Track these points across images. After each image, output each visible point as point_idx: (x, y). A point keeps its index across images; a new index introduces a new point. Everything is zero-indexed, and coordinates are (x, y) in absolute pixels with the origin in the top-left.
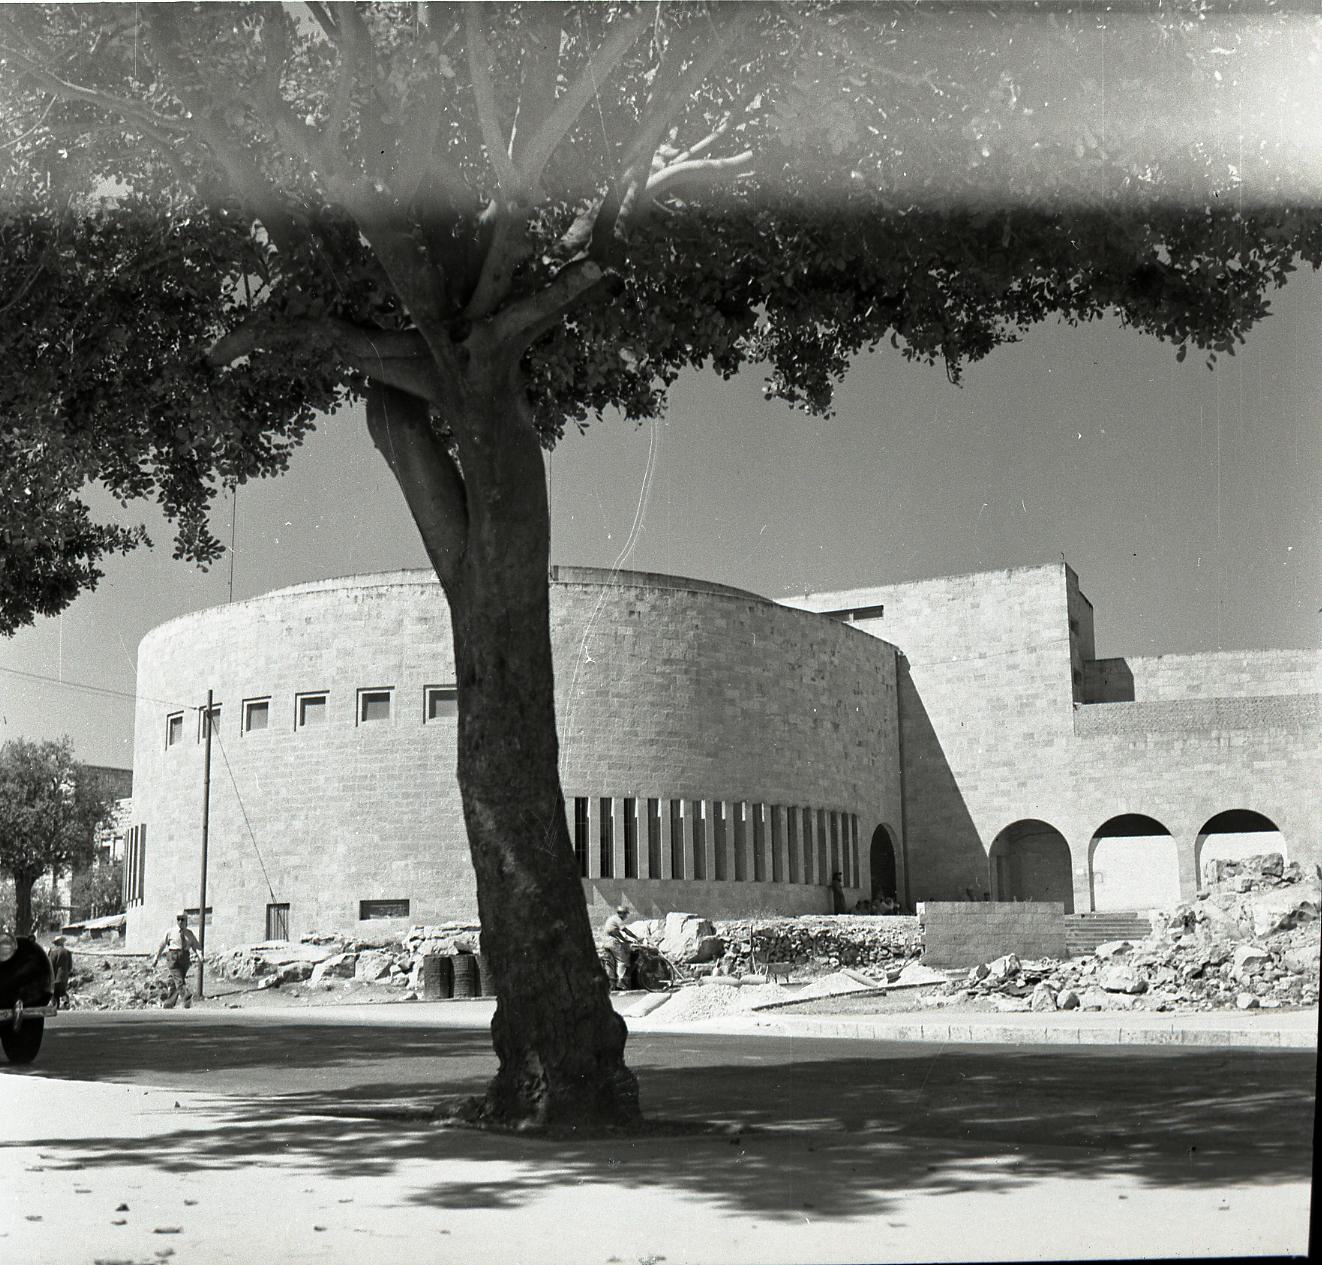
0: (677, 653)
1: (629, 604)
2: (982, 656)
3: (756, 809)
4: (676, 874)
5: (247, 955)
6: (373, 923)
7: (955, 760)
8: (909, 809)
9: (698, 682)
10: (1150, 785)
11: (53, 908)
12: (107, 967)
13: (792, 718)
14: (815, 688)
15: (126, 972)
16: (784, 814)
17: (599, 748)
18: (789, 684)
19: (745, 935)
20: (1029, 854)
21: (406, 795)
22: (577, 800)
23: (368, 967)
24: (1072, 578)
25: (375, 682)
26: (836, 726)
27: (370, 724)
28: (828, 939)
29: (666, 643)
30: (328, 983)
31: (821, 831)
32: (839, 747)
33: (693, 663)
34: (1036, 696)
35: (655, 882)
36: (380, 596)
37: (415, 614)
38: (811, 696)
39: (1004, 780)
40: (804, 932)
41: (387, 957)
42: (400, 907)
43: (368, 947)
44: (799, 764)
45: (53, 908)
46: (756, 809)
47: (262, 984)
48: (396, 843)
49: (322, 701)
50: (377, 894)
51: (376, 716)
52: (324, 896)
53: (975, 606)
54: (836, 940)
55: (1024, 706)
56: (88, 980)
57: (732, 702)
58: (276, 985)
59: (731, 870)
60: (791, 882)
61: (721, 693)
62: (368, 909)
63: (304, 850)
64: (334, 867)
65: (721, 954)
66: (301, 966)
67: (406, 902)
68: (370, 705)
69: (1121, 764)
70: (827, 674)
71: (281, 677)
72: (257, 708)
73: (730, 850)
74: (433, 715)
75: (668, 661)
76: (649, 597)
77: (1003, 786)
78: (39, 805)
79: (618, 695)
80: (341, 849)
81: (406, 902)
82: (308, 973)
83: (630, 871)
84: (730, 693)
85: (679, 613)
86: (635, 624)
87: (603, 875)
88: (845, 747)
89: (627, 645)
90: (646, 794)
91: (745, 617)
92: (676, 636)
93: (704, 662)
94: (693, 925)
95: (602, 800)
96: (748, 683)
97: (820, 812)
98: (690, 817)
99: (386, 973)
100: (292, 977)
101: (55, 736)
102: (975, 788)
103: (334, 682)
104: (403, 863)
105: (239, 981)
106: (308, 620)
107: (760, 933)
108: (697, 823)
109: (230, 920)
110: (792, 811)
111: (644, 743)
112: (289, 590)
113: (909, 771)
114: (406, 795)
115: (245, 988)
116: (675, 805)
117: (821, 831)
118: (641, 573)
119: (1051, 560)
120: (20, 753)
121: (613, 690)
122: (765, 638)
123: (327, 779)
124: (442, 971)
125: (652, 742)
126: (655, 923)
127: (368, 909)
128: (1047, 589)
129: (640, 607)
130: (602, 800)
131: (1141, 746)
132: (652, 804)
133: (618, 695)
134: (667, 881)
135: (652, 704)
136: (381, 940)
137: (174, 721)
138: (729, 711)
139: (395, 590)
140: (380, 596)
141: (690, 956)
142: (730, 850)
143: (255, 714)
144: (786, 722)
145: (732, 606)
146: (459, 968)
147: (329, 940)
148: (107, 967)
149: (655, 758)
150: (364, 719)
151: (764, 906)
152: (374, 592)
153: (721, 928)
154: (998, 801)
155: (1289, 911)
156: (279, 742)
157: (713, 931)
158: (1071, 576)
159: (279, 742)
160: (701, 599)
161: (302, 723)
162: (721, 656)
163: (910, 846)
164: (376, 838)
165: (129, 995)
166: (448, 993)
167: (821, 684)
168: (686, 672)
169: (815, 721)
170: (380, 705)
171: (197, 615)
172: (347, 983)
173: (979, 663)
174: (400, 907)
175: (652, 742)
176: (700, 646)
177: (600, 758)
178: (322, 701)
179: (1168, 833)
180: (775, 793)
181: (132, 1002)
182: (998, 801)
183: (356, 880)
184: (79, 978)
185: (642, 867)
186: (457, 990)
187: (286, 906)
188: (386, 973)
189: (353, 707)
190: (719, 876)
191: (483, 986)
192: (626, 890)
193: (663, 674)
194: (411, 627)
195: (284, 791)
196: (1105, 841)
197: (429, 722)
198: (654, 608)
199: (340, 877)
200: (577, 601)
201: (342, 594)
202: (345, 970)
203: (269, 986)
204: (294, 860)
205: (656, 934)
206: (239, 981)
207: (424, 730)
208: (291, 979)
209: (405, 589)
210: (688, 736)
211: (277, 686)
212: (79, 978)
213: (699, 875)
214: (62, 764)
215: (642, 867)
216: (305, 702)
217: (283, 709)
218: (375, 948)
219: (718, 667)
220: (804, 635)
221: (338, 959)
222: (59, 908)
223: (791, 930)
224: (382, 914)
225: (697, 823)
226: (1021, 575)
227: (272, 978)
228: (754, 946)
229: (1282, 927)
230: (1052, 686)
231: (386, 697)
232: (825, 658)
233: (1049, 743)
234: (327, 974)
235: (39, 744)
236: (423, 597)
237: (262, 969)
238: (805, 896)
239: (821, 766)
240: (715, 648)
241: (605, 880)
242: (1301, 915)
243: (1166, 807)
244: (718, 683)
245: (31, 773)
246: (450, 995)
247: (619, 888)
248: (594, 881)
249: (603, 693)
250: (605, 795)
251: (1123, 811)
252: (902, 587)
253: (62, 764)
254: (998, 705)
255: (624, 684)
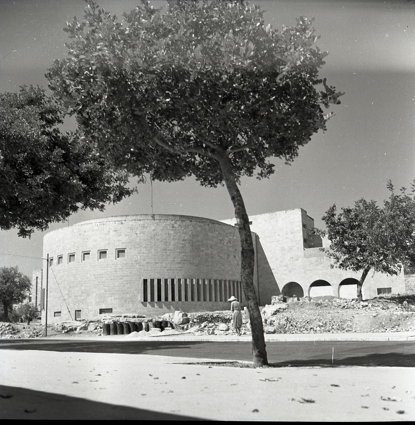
0: (186, 238)
1: (173, 225)
2: (279, 235)
3: (210, 281)
4: (186, 299)
5: (60, 324)
6: (103, 315)
7: (272, 265)
8: (260, 280)
9: (192, 246)
10: (325, 271)
11: (36, 312)
12: (24, 328)
13: (221, 255)
14: (228, 246)
15: (29, 329)
16: (218, 282)
17: (164, 265)
18: (220, 245)
19: (195, 317)
20: (131, 305)
21: (111, 279)
22: (158, 280)
23: (91, 327)
24: (304, 212)
25: (103, 248)
26: (235, 257)
27: (102, 260)
28: (218, 318)
29: (183, 235)
30: (81, 331)
31: (230, 287)
32: (236, 262)
33: (191, 240)
34: (293, 246)
35: (180, 302)
36: (104, 224)
37: (114, 229)
38: (226, 248)
39: (285, 270)
40: (212, 316)
41: (97, 324)
42: (110, 310)
43: (92, 322)
44: (223, 268)
45: (36, 312)
46: (210, 281)
47: (63, 332)
48: (108, 293)
49: (89, 254)
50: (104, 307)
51: (103, 258)
52: (90, 308)
53: (277, 221)
54: (221, 318)
55: (290, 249)
56: (18, 332)
57: (203, 251)
58: (67, 332)
59: (202, 298)
60: (220, 301)
61: (199, 249)
62: (102, 311)
63: (85, 295)
64: (92, 300)
65: (188, 322)
66: (74, 327)
67: (111, 309)
68: (102, 254)
69: (317, 265)
70: (232, 242)
71: (78, 247)
72: (72, 256)
73: (202, 292)
74: (118, 257)
75: (184, 240)
76: (178, 223)
77: (285, 272)
78: (8, 284)
79: (169, 250)
80: (94, 294)
81: (111, 309)
82: (76, 329)
83: (173, 299)
84: (202, 249)
85: (187, 227)
86: (174, 230)
87: (172, 300)
88: (238, 262)
89: (172, 236)
90: (177, 277)
91: (207, 227)
92: (186, 233)
93: (194, 240)
94: (181, 314)
95: (165, 279)
96: (207, 245)
97: (229, 281)
98: (190, 284)
99: (96, 329)
100: (72, 330)
101: (14, 266)
102: (277, 273)
103: (92, 249)
104: (110, 298)
105: (58, 331)
106: (85, 232)
107: (199, 316)
108: (192, 285)
109: (66, 315)
110: (220, 281)
111: (177, 263)
112: (79, 224)
113: (260, 268)
114: (111, 279)
115: (59, 333)
116: (186, 280)
117: (230, 287)
118: (178, 215)
119: (297, 208)
120: (5, 271)
121: (168, 249)
122: (212, 233)
123: (90, 275)
124: (107, 328)
125: (179, 263)
126: (171, 314)
127: (102, 311)
128: (296, 216)
129: (175, 225)
130: (165, 279)
131: (322, 260)
132: (179, 280)
133: (169, 250)
134: (183, 302)
135: (179, 252)
136: (96, 320)
137: (59, 258)
138: (202, 253)
139: (108, 223)
140: (104, 224)
141: (180, 323)
142: (202, 292)
143: (72, 257)
144: (219, 256)
145: (202, 224)
146: (111, 327)
147: (83, 320)
148: (24, 328)
149: (180, 267)
150: (100, 258)
151: (203, 309)
152: (102, 224)
153: (189, 315)
154: (283, 277)
155: (275, 310)
156: (78, 265)
157: (187, 316)
158: (304, 212)
159: (78, 265)
160: (193, 223)
161: (84, 260)
162: (199, 239)
163: (260, 290)
164: (103, 291)
165: (28, 336)
166: (109, 333)
167: (229, 245)
168: (189, 243)
169: (228, 255)
170: (105, 254)
171: (56, 231)
172: (86, 331)
173: (278, 237)
174: (110, 310)
175: (179, 263)
176: (193, 236)
177: (165, 268)
178: (89, 254)
179: (330, 285)
180: (215, 276)
181: (30, 337)
182: (283, 277)
183: (98, 303)
184: (16, 331)
185: (177, 298)
186: (111, 333)
187: (80, 311)
188: (96, 329)
189: (97, 255)
190: (199, 300)
191: (125, 332)
192: (172, 305)
193: (182, 244)
194: (112, 233)
195: (79, 279)
196: (343, 286)
197: (117, 259)
198: (179, 225)
199: (94, 302)
200: (158, 224)
201: (94, 224)
202: (85, 328)
203: (65, 333)
204: (82, 298)
205: (171, 317)
206: (58, 331)
207: (116, 261)
208: (71, 330)
209: (111, 222)
210: (189, 261)
211: (77, 250)
212: (16, 331)
213: (193, 300)
214: (15, 273)
215: (177, 298)
216: (84, 254)
217: (78, 256)
218: (94, 322)
219: (198, 241)
220: (224, 231)
221: (84, 325)
222: (37, 312)
223: (208, 315)
224: (105, 312)
225: (192, 285)
226: (289, 212)
227: (66, 331)
228: (197, 320)
229: (274, 314)
230: (298, 243)
231: (105, 252)
232: (230, 237)
233: (297, 260)
234: (80, 329)
235: (9, 268)
236: (116, 224)
237: (64, 328)
238: (225, 305)
239: (230, 268)
240: (198, 236)
241: (166, 302)
242: (279, 311)
243: (330, 277)
244: (198, 246)
245: (9, 276)
246: (109, 334)
247: (170, 304)
248: (156, 302)
249: (165, 249)
250: (166, 278)
251: (318, 279)
252: (257, 216)
253: (15, 273)
254: (283, 249)
255: (171, 247)
